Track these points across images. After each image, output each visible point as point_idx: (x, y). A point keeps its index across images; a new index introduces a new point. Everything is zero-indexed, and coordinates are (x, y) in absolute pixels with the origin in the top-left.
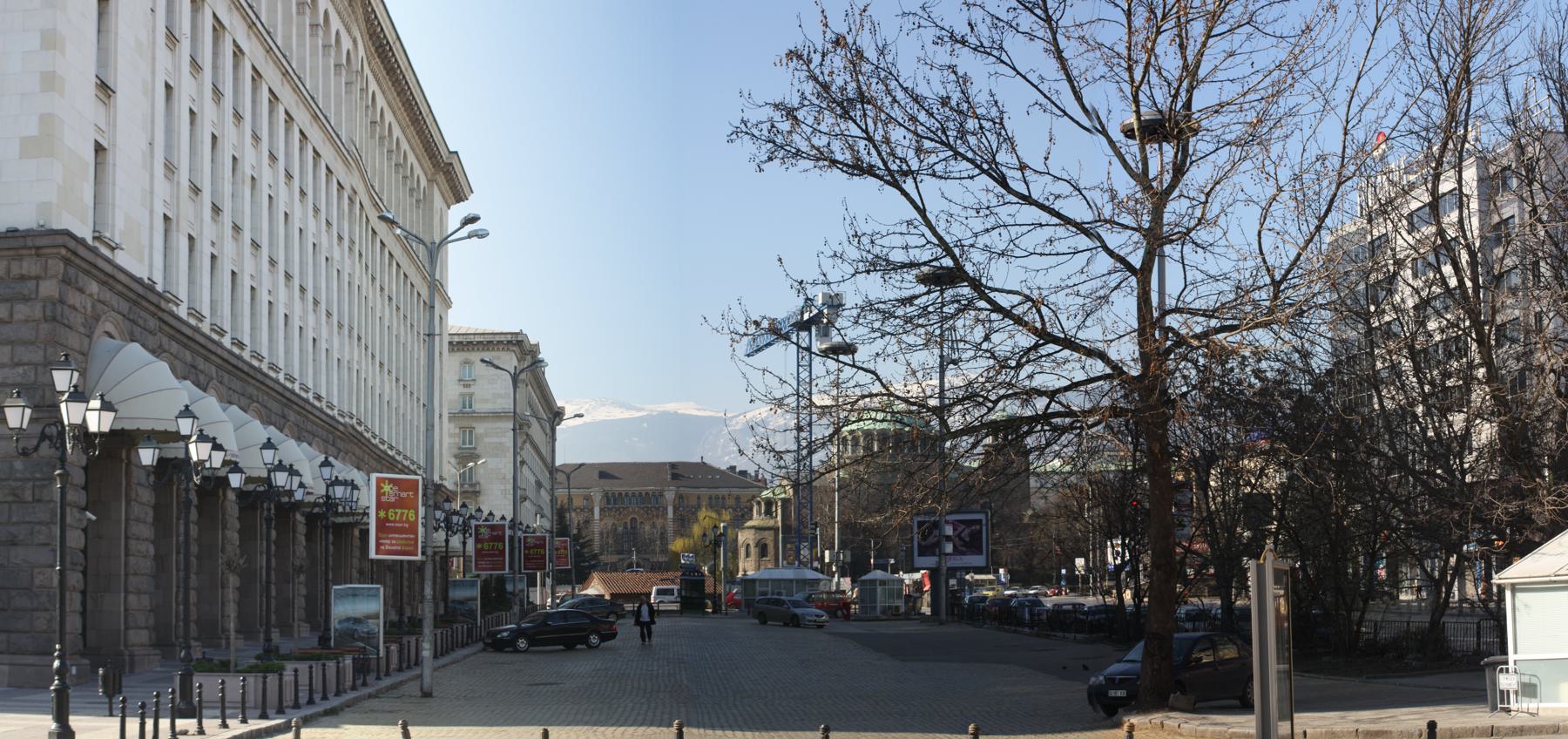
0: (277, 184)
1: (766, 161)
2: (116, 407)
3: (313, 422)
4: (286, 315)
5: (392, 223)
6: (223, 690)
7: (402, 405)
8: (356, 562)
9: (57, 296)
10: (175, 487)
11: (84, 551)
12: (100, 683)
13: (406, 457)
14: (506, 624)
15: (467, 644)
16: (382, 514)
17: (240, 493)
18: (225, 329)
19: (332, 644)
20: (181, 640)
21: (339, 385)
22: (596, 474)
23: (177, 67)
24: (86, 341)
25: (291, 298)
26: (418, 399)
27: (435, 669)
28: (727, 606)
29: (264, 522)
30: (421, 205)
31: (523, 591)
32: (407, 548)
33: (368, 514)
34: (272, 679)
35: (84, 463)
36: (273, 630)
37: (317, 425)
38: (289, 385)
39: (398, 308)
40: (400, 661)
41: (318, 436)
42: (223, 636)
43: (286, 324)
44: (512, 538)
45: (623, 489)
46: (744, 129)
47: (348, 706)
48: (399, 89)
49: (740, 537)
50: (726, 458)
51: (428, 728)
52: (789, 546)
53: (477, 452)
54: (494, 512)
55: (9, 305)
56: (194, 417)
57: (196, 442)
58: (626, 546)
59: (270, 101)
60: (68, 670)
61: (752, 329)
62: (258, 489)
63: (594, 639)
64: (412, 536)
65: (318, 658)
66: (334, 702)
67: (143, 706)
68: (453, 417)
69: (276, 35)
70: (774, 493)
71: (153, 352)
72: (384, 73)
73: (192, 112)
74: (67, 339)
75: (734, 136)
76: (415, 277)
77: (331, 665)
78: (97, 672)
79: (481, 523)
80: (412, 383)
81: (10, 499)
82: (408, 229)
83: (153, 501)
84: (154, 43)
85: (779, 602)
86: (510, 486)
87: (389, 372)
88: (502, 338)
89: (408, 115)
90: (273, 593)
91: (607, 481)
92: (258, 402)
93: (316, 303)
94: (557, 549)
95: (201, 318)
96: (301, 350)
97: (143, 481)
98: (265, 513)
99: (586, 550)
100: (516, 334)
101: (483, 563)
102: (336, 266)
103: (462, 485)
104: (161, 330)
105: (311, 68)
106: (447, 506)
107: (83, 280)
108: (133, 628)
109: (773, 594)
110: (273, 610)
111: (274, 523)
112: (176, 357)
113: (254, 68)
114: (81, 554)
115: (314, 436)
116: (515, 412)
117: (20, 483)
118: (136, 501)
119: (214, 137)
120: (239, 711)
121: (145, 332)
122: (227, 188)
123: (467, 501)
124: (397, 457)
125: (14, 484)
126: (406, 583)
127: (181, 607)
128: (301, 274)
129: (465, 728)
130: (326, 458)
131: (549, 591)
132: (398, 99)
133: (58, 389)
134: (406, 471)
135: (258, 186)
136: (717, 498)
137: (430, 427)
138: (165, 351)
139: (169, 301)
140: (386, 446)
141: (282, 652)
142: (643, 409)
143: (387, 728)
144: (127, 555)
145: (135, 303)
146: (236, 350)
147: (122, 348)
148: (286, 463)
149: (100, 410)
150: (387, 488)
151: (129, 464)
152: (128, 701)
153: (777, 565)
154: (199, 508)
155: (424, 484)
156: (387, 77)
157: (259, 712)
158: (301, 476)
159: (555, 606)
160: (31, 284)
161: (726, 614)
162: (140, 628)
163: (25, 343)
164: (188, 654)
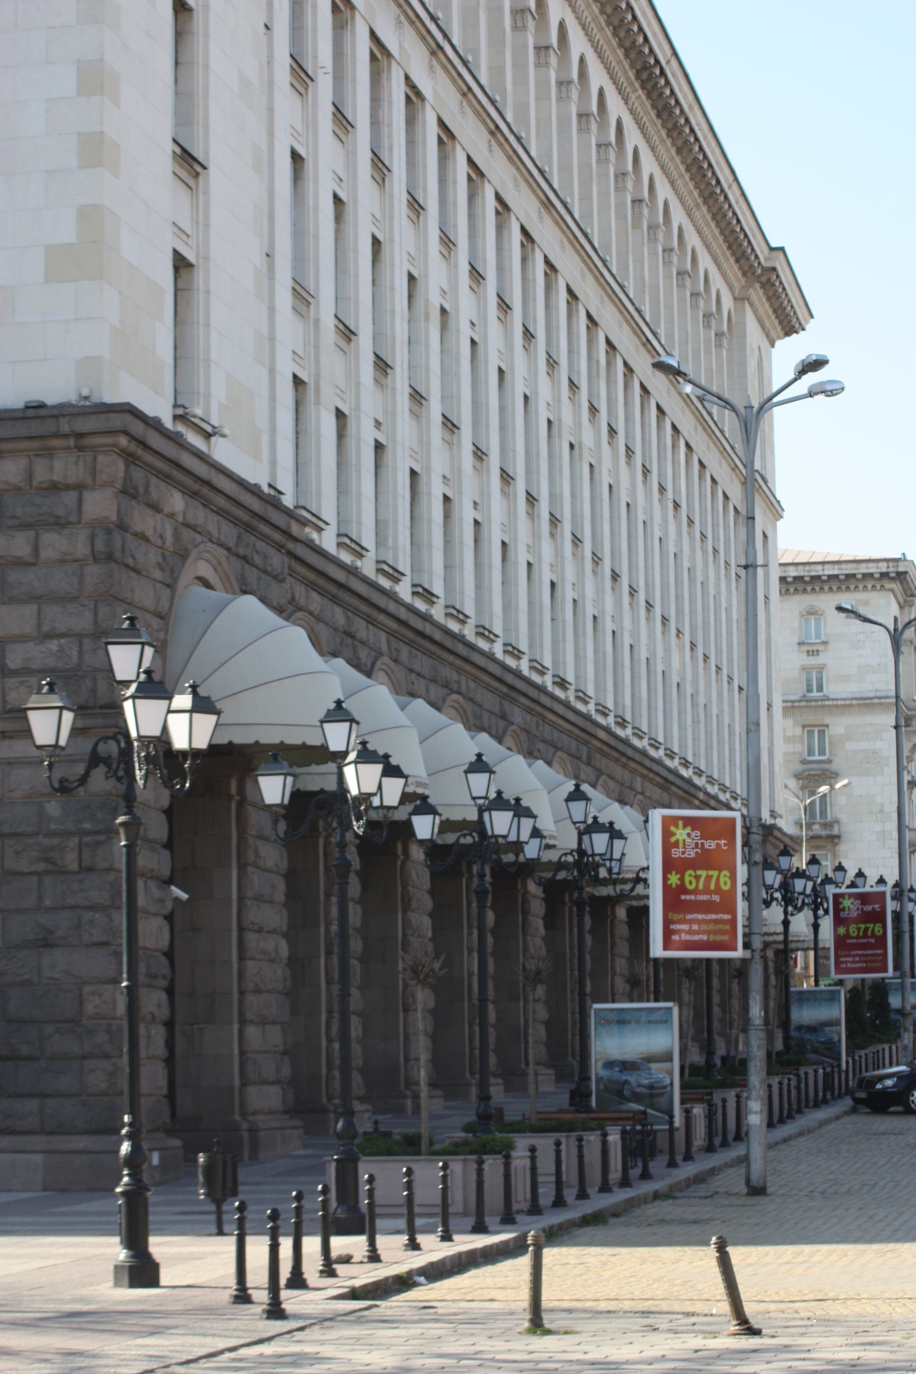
0: (485, 320)
2: (219, 706)
3: (553, 725)
4: (504, 544)
6: (409, 1186)
7: (702, 688)
8: (621, 964)
9: (114, 518)
10: (321, 841)
11: (169, 954)
12: (201, 1178)
13: (711, 780)
14: (891, 1065)
15: (825, 1101)
16: (674, 879)
17: (433, 848)
18: (401, 569)
19: (594, 1103)
20: (337, 1101)
21: (596, 662)
23: (310, 123)
24: (166, 593)
25: (511, 513)
26: (730, 678)
27: (771, 1146)
29: (474, 897)
30: (725, 342)
33: (645, 881)
34: (493, 1165)
35: (165, 802)
36: (492, 1080)
37: (561, 730)
38: (511, 662)
39: (691, 522)
41: (562, 749)
42: (408, 1093)
43: (504, 559)
47: (616, 1215)
48: (679, 143)
51: (761, 1250)
53: (833, 767)
54: (866, 871)
55: (31, 534)
56: (352, 721)
57: (356, 762)
59: (470, 179)
60: (147, 1159)
62: (463, 841)
64: (726, 917)
65: (570, 1128)
66: (599, 1202)
67: (275, 1216)
71: (279, 610)
72: (653, 114)
73: (337, 200)
74: (133, 592)
76: (718, 467)
77: (592, 1139)
78: (196, 1160)
79: (843, 890)
80: (719, 651)
81: (41, 867)
82: (703, 383)
83: (284, 865)
84: (271, 83)
86: (892, 826)
88: (872, 569)
89: (696, 187)
90: (492, 1018)
92: (459, 693)
93: (554, 521)
95: (359, 551)
96: (530, 603)
97: (268, 831)
98: (476, 881)
100: (896, 560)
101: (848, 961)
102: (587, 458)
103: (809, 826)
104: (292, 573)
105: (538, 120)
106: (784, 862)
107: (158, 488)
108: (254, 1083)
110: (492, 1046)
112: (319, 619)
113: (442, 123)
114: (165, 961)
115: (557, 748)
116: (897, 697)
117: (56, 841)
118: (257, 867)
119: (376, 242)
120: (439, 1220)
121: (263, 576)
122: (401, 330)
123: (819, 853)
124: (697, 781)
125: (46, 841)
126: (716, 999)
127: (337, 1046)
128: (528, 472)
130: (577, 786)
132: (678, 160)
133: (120, 676)
137: (752, 728)
138: (300, 609)
139: (304, 523)
141: (508, 1118)
144: (242, 958)
145: (248, 527)
146: (420, 605)
147: (222, 607)
148: (509, 795)
149: (191, 711)
150: (681, 834)
151: (242, 802)
152: (251, 1208)
154: (363, 876)
156: (659, 122)
157: (471, 1221)
160: (70, 498)
162: (266, 1082)
163: (61, 599)
164: (349, 1125)
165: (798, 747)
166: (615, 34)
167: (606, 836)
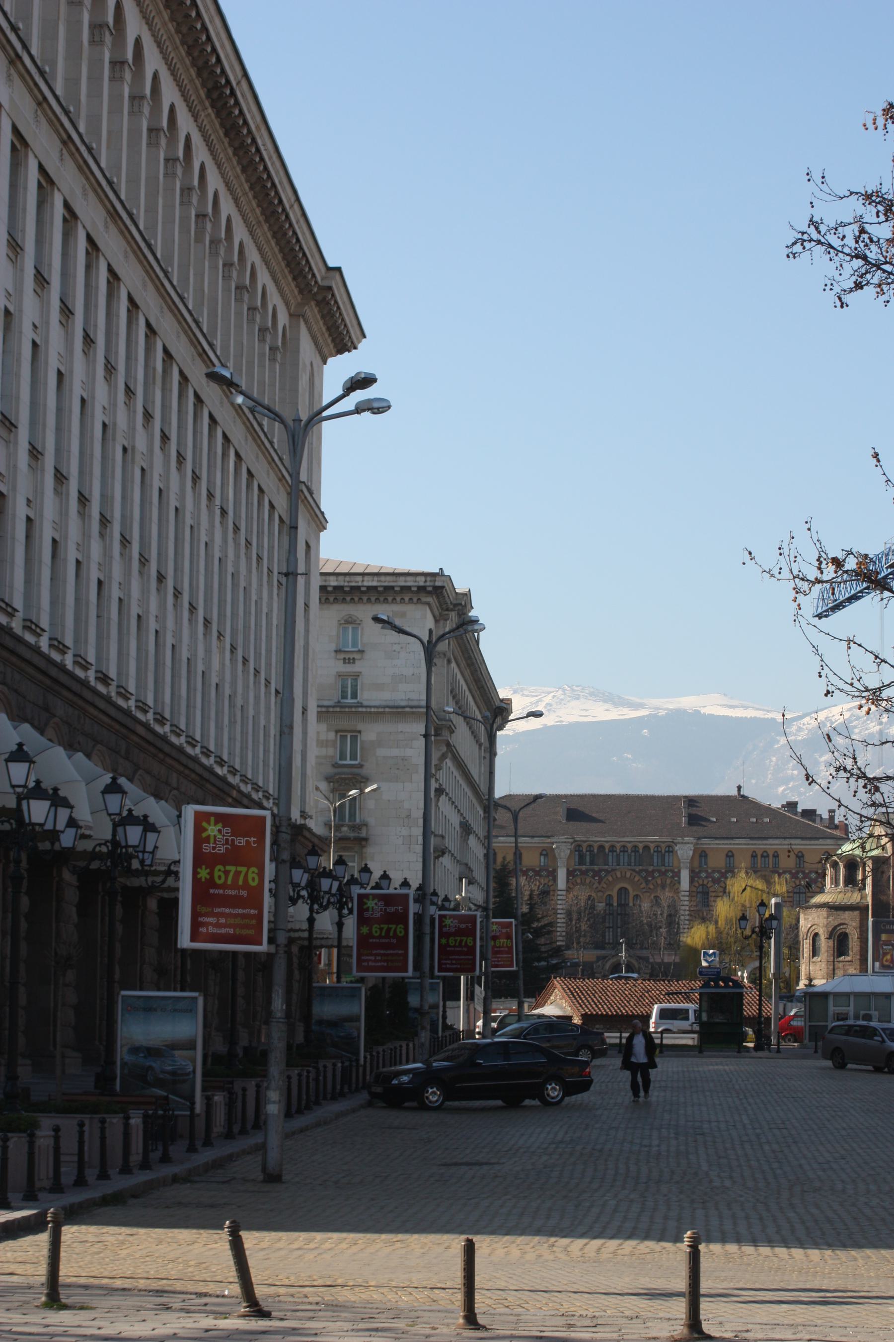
0: (48, 323)
1: (851, 290)
5: (228, 384)
7: (240, 690)
13: (245, 779)
14: (407, 1062)
15: (342, 1095)
16: (204, 873)
19: (118, 1088)
22: (561, 814)
27: (288, 1136)
28: (779, 1037)
30: (279, 357)
31: (436, 1006)
32: (245, 932)
33: (176, 873)
38: (56, 656)
39: (236, 529)
40: (230, 1120)
44: (419, 919)
45: (607, 839)
46: (815, 236)
47: (135, 1196)
49: (802, 922)
50: (781, 789)
52: (884, 937)
53: (364, 772)
54: (392, 874)
58: (609, 936)
61: (829, 572)
63: (553, 1091)
66: (119, 1183)
68: (324, 713)
69: (55, 78)
70: (863, 848)
72: (221, 133)
75: (798, 248)
76: (266, 477)
77: (115, 1121)
79: (368, 891)
80: (258, 654)
85: (867, 1032)
86: (418, 831)
87: (220, 635)
88: (410, 582)
90: (23, 1000)
91: (578, 824)
93: (105, 521)
94: (494, 938)
99: (542, 941)
102: (140, 462)
103: (338, 828)
105: (109, 133)
106: (312, 862)
109: (857, 1017)
111: (25, 883)
116: (428, 707)
123: (344, 854)
126: (241, 991)
128: (81, 472)
129: (335, 1236)
130: (114, 779)
131: (480, 1008)
134: (245, 801)
135: (42, 357)
136: (765, 855)
137: (286, 730)
140: (212, 760)
142: (641, 706)
143: (205, 1235)
148: (47, 785)
150: (212, 830)
153: (864, 969)
155: (274, 825)
156: (226, 141)
158: (72, 807)
159: (489, 1033)
161: (778, 1051)
165: (330, 751)
166: (189, 54)
167: (140, 829)
